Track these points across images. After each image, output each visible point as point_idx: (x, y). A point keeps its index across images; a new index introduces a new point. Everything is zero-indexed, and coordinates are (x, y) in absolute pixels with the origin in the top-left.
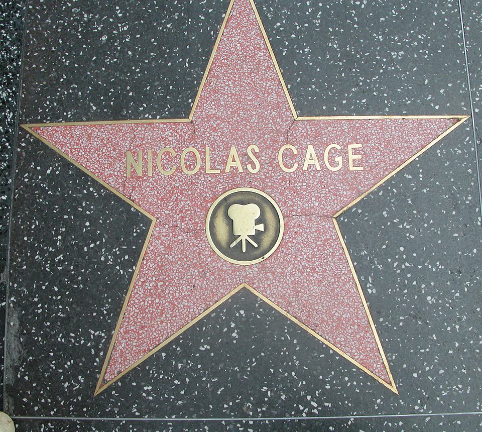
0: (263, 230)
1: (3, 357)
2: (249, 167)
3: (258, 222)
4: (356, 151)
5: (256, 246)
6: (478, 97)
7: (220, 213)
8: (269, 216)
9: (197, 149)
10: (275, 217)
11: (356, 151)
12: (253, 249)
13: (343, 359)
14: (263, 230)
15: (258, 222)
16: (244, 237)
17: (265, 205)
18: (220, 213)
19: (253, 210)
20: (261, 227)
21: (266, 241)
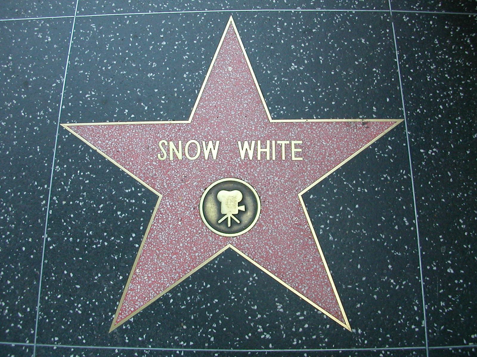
0: (244, 210)
1: (305, 347)
2: (159, 155)
3: (240, 204)
4: (296, 146)
5: (239, 222)
6: (322, 228)
7: (211, 198)
8: (249, 200)
9: (192, 139)
10: (254, 203)
11: (296, 146)
12: (234, 225)
13: (262, 87)
14: (244, 210)
15: (240, 204)
16: (229, 215)
17: (247, 194)
18: (211, 198)
19: (237, 195)
20: (242, 208)
21: (246, 218)
